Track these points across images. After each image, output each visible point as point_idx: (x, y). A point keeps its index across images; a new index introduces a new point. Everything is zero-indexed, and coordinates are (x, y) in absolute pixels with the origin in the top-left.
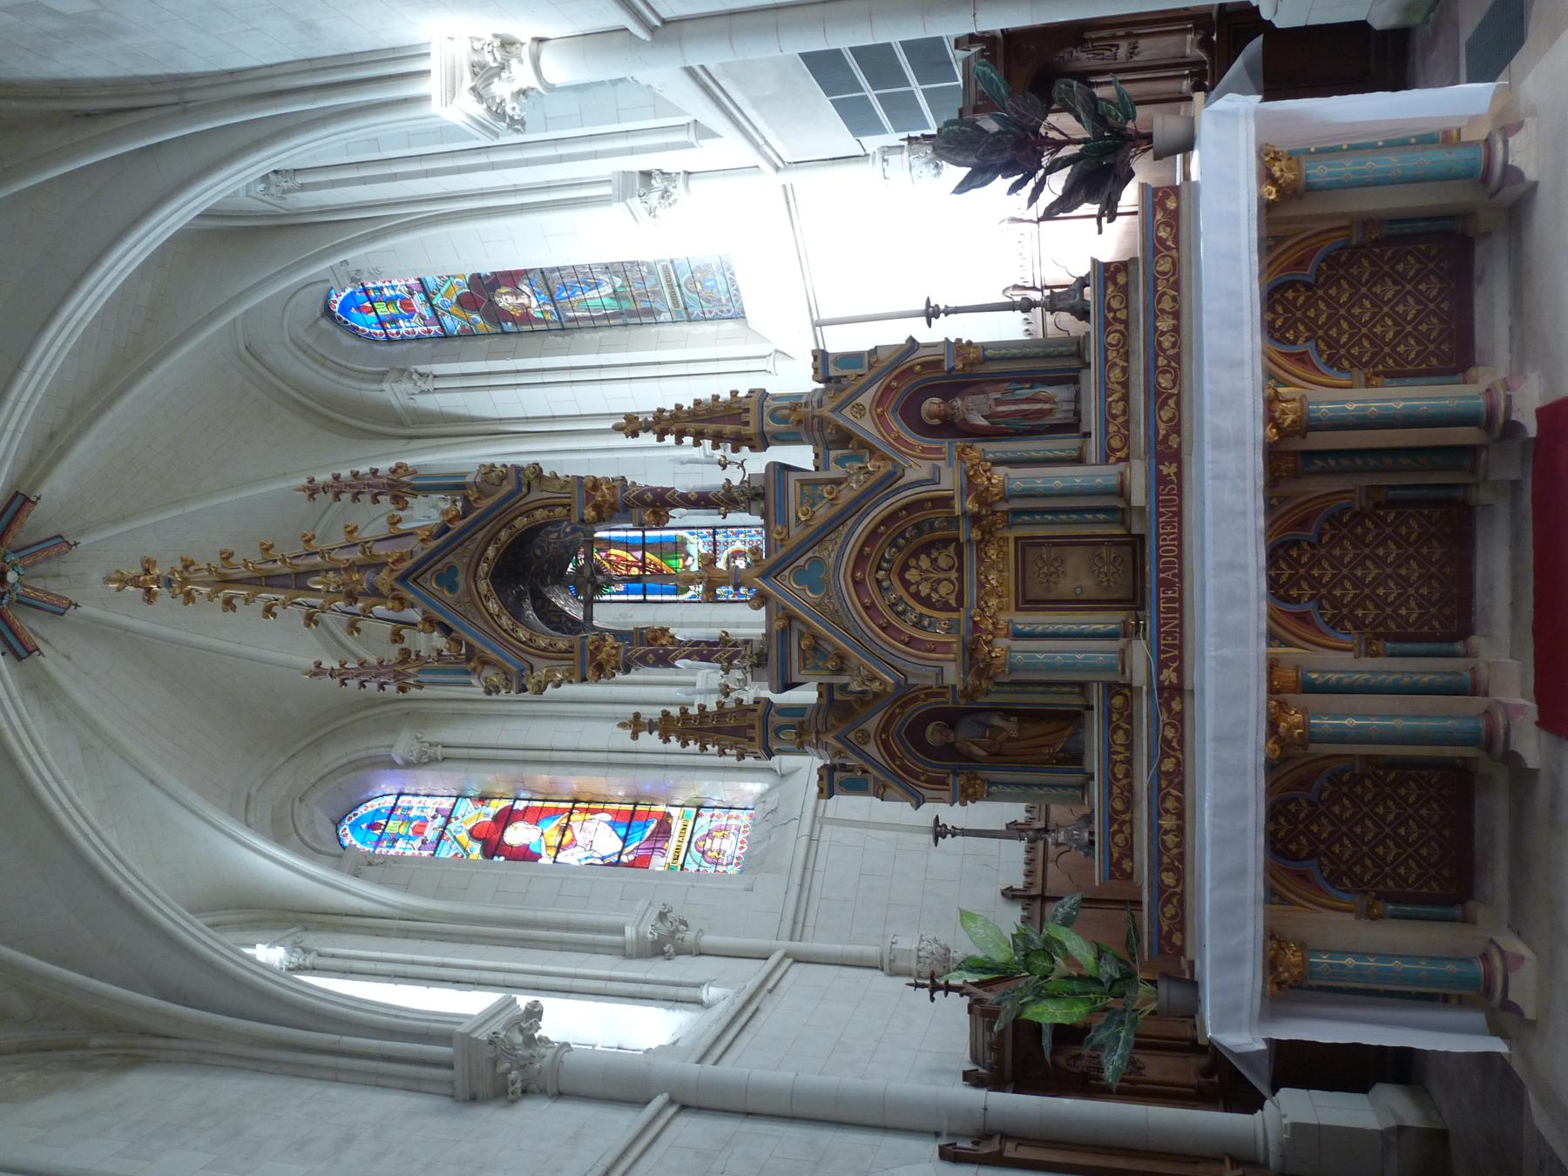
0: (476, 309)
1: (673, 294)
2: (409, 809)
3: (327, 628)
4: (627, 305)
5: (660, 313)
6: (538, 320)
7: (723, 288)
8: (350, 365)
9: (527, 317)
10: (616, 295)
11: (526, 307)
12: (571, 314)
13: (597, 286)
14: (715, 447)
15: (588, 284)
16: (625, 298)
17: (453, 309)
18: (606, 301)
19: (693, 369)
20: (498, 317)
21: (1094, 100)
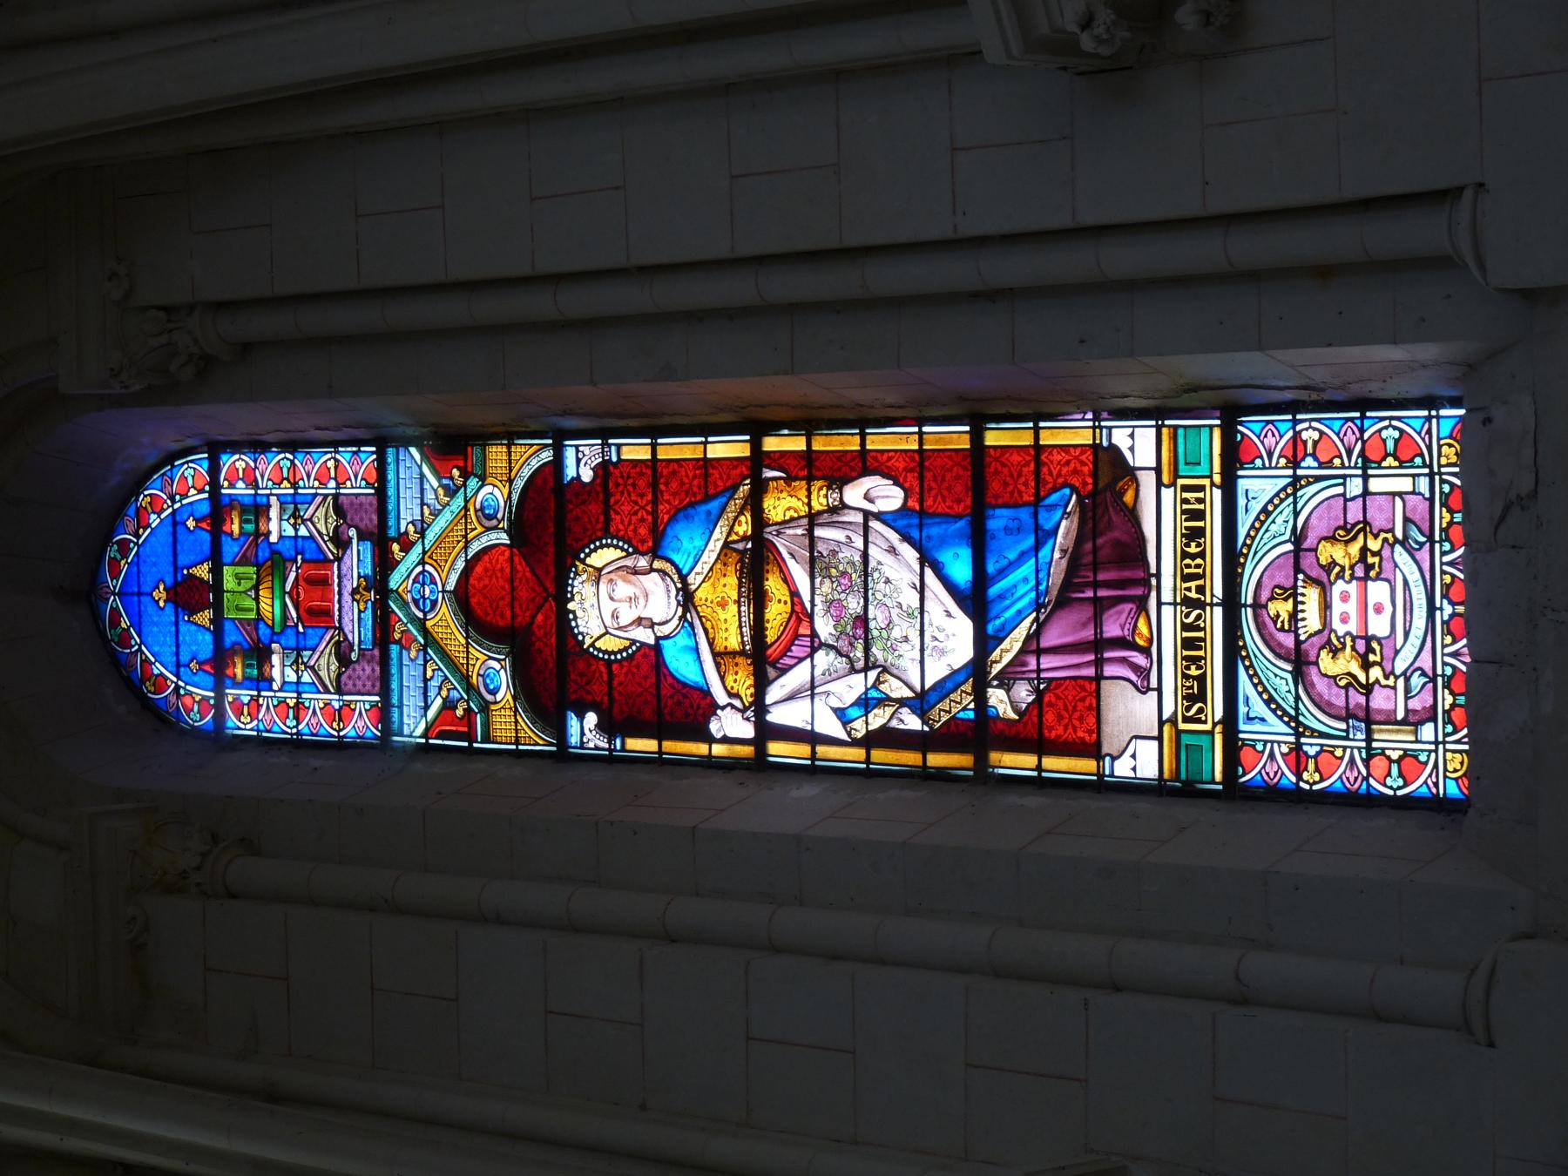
17: (445, 622)
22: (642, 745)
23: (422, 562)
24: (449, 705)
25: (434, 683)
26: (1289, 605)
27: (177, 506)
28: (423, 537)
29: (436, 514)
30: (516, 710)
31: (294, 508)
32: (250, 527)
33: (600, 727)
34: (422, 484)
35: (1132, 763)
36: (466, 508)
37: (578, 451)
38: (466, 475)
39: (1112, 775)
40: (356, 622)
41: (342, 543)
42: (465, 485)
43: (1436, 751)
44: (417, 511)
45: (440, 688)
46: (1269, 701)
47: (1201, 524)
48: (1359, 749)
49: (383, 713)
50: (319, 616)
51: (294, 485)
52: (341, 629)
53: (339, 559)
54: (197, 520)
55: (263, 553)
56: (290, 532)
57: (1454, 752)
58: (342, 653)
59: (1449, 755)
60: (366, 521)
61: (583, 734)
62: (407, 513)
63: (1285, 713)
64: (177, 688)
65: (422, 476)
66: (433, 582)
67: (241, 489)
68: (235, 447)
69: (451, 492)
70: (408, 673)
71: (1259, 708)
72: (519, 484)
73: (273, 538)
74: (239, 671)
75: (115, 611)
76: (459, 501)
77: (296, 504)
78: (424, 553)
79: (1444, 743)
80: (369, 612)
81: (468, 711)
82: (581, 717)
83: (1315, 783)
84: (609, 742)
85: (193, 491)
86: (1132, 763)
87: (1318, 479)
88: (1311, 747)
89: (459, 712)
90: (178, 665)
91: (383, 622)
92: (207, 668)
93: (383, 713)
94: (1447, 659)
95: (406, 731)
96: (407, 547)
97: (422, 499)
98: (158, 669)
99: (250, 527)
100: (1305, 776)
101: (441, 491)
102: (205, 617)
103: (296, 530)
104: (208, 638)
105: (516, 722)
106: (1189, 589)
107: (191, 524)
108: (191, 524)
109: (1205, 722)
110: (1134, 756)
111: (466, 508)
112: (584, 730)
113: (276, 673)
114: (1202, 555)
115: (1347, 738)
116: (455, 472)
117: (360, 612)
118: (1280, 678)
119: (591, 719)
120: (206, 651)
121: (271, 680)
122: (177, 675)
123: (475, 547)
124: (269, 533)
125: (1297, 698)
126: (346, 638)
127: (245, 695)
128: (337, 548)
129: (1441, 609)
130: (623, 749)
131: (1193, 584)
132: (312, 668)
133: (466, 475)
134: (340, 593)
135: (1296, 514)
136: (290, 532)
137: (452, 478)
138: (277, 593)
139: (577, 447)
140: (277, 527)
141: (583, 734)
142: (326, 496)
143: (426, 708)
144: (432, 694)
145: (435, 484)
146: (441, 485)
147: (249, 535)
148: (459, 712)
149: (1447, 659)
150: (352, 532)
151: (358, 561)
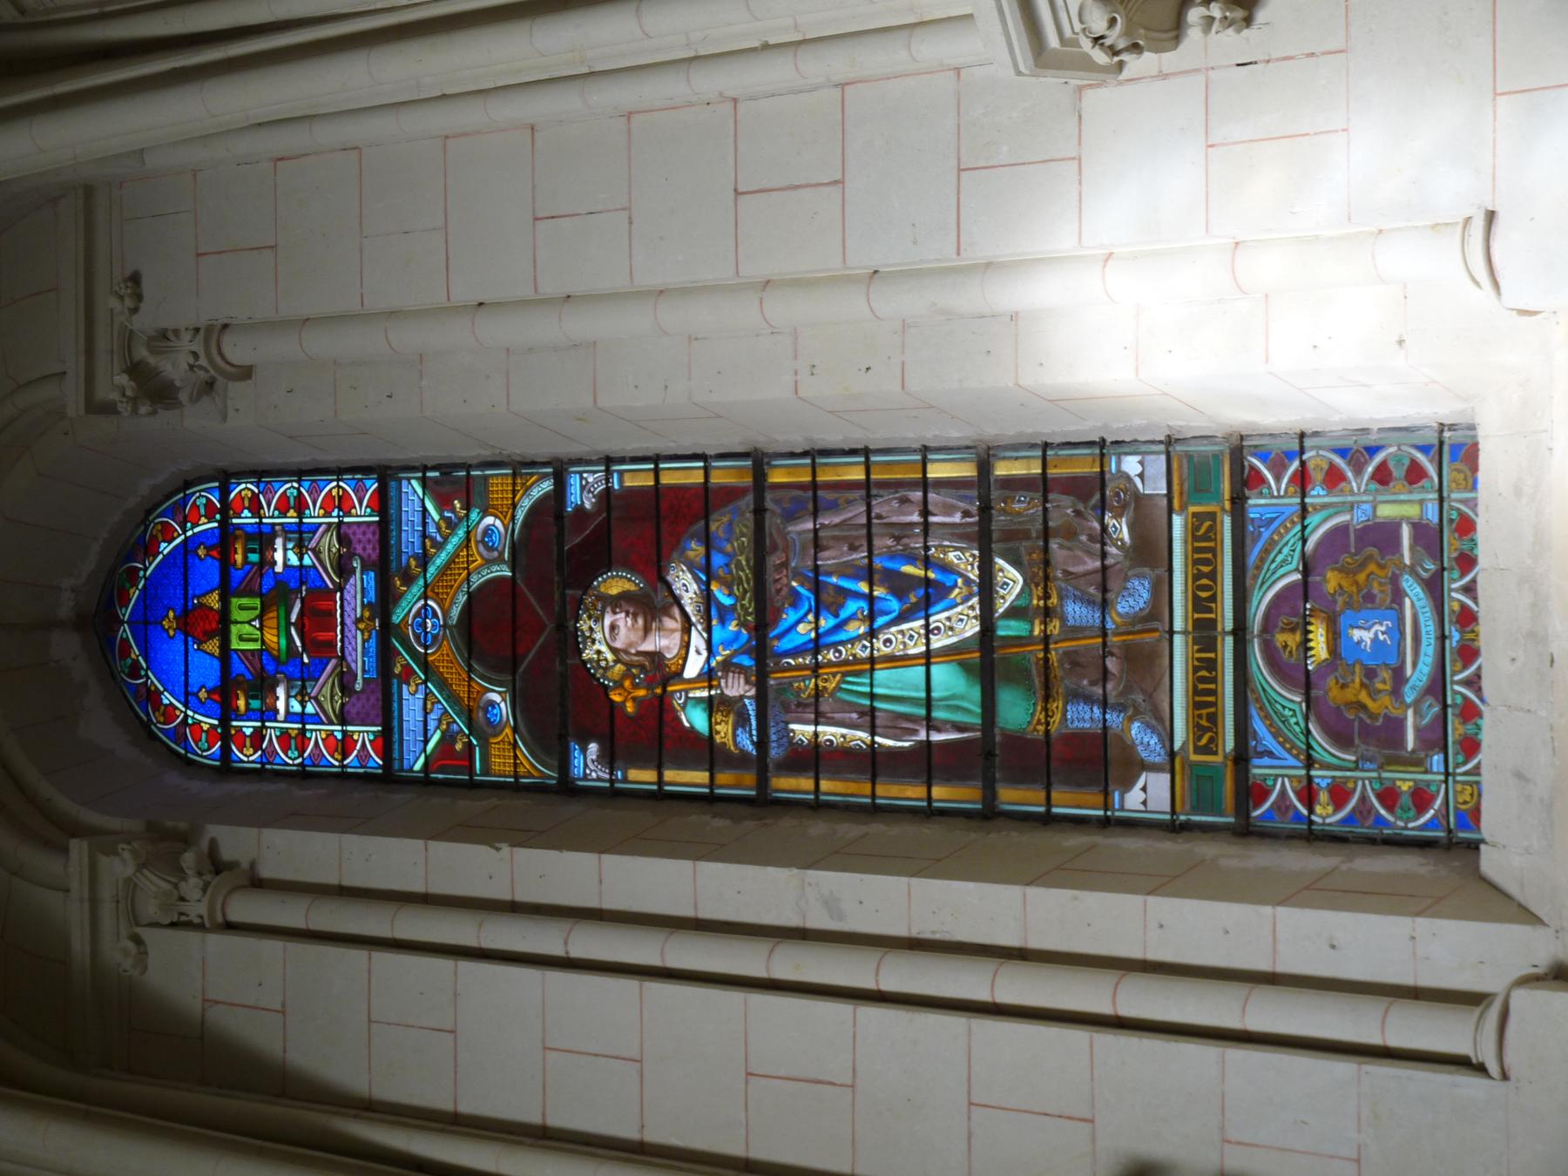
0: (504, 666)
1: (1204, 672)
2: (343, 534)
3: (224, 915)
4: (1015, 711)
5: (1133, 767)
6: (705, 751)
7: (1419, 674)
8: (47, 790)
9: (655, 734)
10: (986, 659)
11: (661, 672)
12: (803, 731)
13: (929, 596)
14: (408, 684)
15: (899, 585)
16: (1019, 676)
17: (445, 656)
18: (946, 678)
19: (1140, 999)
20: (564, 702)
21: (513, 571)
22: (642, 777)
23: (425, 597)
24: (448, 739)
25: (433, 716)
26: (1298, 637)
27: (189, 533)
28: (425, 571)
29: (439, 546)
30: (515, 745)
31: (301, 537)
32: (254, 557)
33: (600, 759)
34: (424, 518)
35: (1142, 796)
36: (468, 539)
37: (582, 478)
38: (468, 507)
39: (1122, 809)
40: (359, 652)
41: (343, 570)
42: (467, 516)
43: (1446, 782)
44: (417, 543)
45: (440, 720)
46: (1276, 734)
47: (1212, 655)
48: (1370, 780)
49: (387, 742)
50: (322, 649)
51: (301, 515)
52: (343, 658)
53: (341, 589)
54: (208, 549)
55: (268, 583)
56: (294, 560)
57: (1464, 783)
58: (345, 681)
59: (1459, 787)
60: (369, 551)
61: (586, 766)
62: (409, 539)
63: (1294, 746)
64: (186, 716)
65: (425, 510)
66: (435, 615)
67: (246, 518)
68: (243, 474)
69: (452, 526)
70: (411, 704)
71: (1269, 742)
72: (520, 515)
73: (279, 568)
74: (241, 703)
75: (125, 641)
76: (461, 532)
77: (301, 533)
78: (426, 585)
79: (1454, 774)
80: (373, 642)
81: (470, 747)
82: (584, 750)
83: (1328, 816)
84: (611, 774)
85: (203, 520)
86: (1142, 796)
87: (1324, 506)
88: (1322, 777)
89: (459, 746)
90: (187, 694)
91: (386, 655)
92: (216, 697)
93: (387, 742)
94: (1457, 688)
95: (406, 766)
96: (409, 580)
97: (424, 530)
98: (167, 698)
99: (254, 557)
100: (1318, 809)
101: (443, 525)
102: (213, 646)
103: (301, 559)
104: (216, 663)
105: (516, 757)
106: (1200, 716)
107: (202, 552)
108: (202, 552)
109: (1215, 753)
110: (1144, 789)
111: (468, 539)
112: (587, 762)
113: (281, 705)
114: (1214, 680)
115: (1356, 769)
116: (457, 504)
117: (364, 641)
118: (1290, 701)
119: (593, 748)
120: (213, 679)
121: (277, 711)
122: (186, 705)
123: (477, 581)
124: (275, 563)
125: (1308, 733)
126: (349, 666)
127: (248, 727)
128: (340, 577)
129: (1451, 637)
130: (625, 780)
131: (1204, 712)
132: (316, 699)
133: (468, 507)
134: (343, 623)
135: (1304, 541)
136: (294, 560)
137: (453, 510)
138: (283, 623)
139: (581, 473)
140: (283, 556)
141: (586, 766)
142: (330, 524)
143: (426, 742)
144: (432, 725)
145: (436, 517)
146: (442, 517)
147: (253, 564)
148: (459, 746)
149: (1457, 688)
150: (356, 564)
151: (360, 588)
